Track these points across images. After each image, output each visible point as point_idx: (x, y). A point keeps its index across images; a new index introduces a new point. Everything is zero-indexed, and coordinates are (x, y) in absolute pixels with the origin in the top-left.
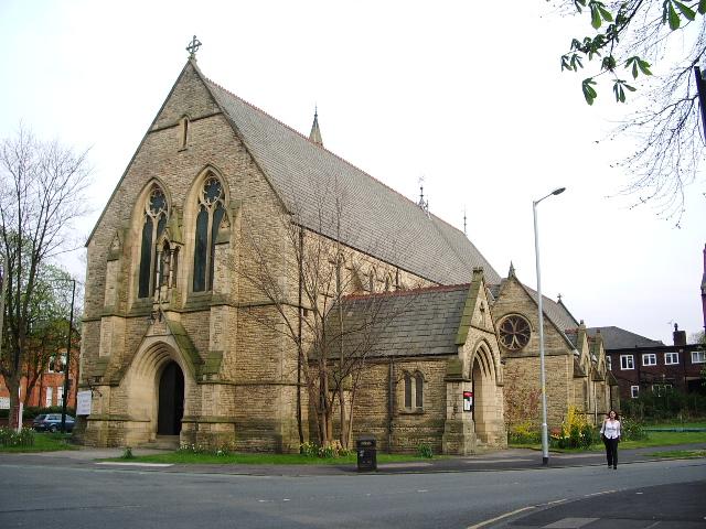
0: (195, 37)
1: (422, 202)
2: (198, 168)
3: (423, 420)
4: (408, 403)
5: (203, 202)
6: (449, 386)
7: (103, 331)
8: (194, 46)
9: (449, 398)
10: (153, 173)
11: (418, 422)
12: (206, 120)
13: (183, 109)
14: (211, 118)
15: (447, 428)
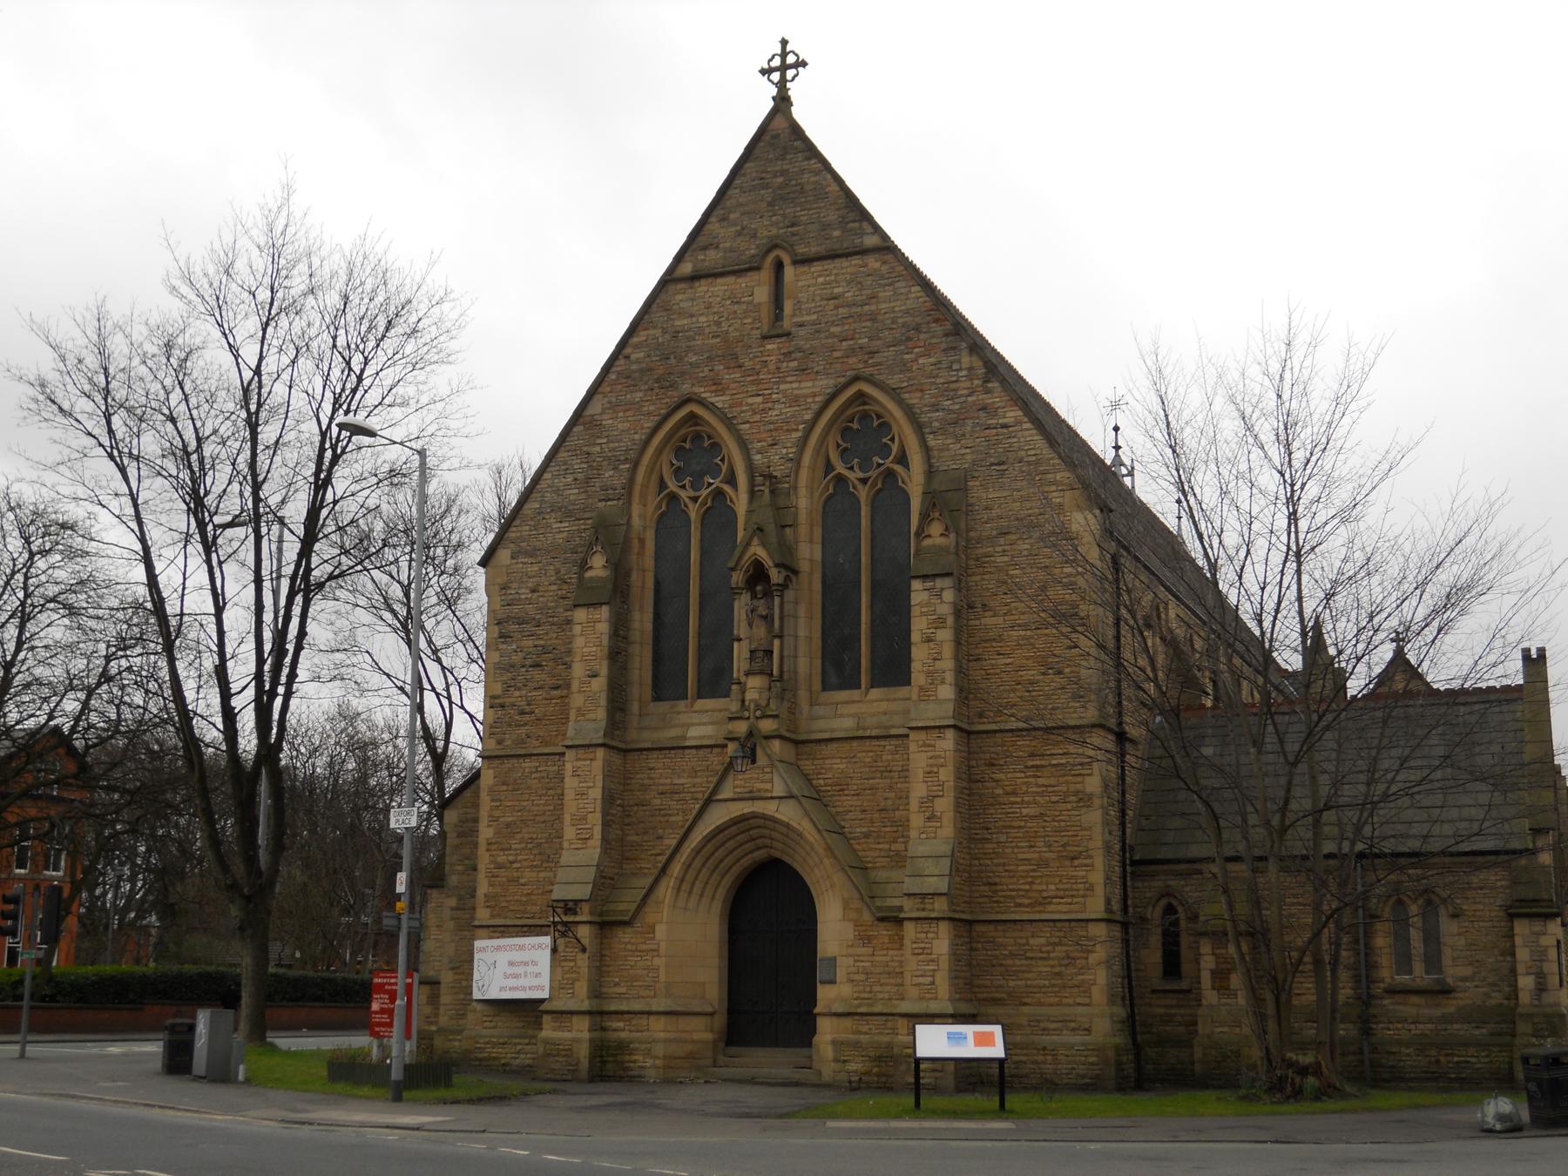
0: (784, 43)
1: (1118, 461)
2: (825, 384)
3: (1450, 1006)
4: (1404, 963)
5: (840, 468)
6: (1521, 928)
7: (570, 783)
8: (783, 67)
9: (1523, 954)
10: (686, 388)
11: (1438, 1012)
12: (844, 262)
13: (767, 228)
14: (856, 261)
15: (1523, 1027)
